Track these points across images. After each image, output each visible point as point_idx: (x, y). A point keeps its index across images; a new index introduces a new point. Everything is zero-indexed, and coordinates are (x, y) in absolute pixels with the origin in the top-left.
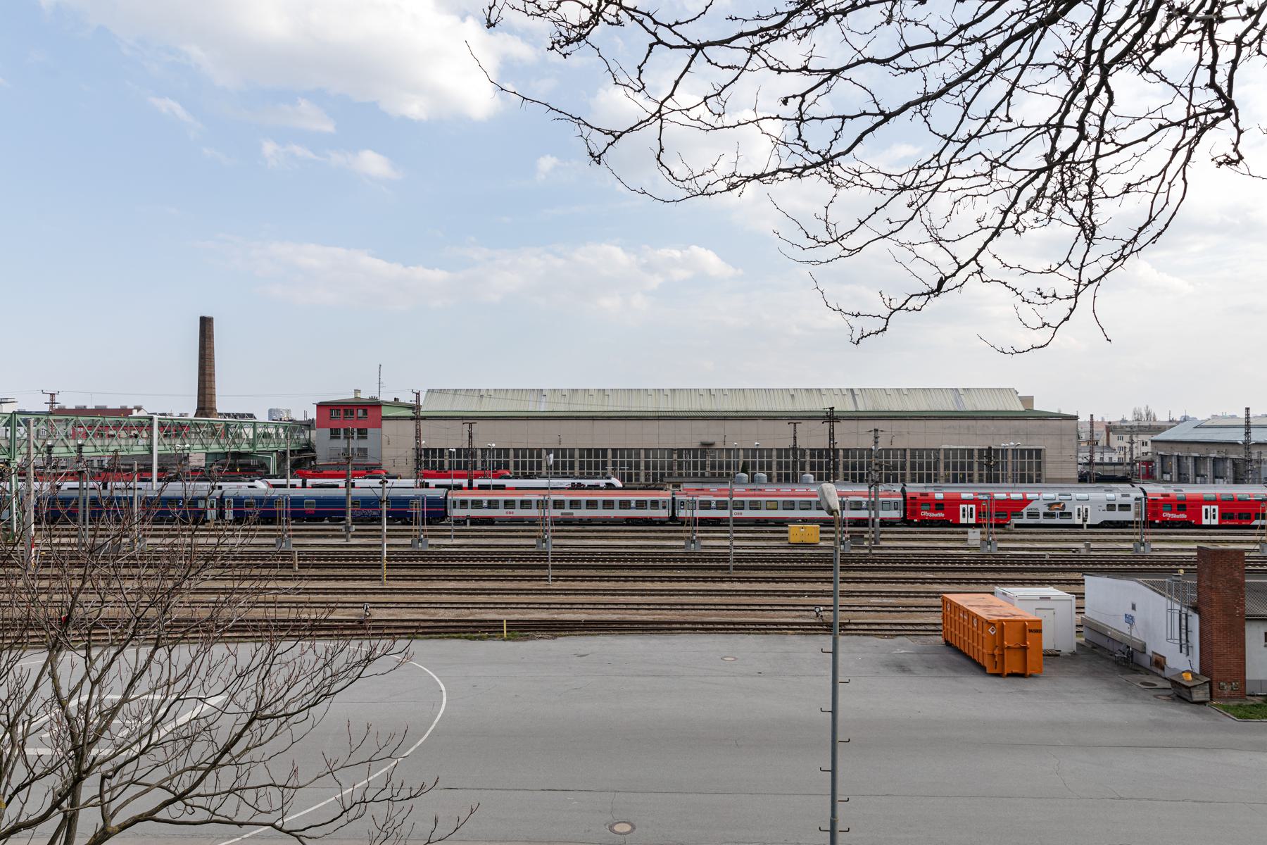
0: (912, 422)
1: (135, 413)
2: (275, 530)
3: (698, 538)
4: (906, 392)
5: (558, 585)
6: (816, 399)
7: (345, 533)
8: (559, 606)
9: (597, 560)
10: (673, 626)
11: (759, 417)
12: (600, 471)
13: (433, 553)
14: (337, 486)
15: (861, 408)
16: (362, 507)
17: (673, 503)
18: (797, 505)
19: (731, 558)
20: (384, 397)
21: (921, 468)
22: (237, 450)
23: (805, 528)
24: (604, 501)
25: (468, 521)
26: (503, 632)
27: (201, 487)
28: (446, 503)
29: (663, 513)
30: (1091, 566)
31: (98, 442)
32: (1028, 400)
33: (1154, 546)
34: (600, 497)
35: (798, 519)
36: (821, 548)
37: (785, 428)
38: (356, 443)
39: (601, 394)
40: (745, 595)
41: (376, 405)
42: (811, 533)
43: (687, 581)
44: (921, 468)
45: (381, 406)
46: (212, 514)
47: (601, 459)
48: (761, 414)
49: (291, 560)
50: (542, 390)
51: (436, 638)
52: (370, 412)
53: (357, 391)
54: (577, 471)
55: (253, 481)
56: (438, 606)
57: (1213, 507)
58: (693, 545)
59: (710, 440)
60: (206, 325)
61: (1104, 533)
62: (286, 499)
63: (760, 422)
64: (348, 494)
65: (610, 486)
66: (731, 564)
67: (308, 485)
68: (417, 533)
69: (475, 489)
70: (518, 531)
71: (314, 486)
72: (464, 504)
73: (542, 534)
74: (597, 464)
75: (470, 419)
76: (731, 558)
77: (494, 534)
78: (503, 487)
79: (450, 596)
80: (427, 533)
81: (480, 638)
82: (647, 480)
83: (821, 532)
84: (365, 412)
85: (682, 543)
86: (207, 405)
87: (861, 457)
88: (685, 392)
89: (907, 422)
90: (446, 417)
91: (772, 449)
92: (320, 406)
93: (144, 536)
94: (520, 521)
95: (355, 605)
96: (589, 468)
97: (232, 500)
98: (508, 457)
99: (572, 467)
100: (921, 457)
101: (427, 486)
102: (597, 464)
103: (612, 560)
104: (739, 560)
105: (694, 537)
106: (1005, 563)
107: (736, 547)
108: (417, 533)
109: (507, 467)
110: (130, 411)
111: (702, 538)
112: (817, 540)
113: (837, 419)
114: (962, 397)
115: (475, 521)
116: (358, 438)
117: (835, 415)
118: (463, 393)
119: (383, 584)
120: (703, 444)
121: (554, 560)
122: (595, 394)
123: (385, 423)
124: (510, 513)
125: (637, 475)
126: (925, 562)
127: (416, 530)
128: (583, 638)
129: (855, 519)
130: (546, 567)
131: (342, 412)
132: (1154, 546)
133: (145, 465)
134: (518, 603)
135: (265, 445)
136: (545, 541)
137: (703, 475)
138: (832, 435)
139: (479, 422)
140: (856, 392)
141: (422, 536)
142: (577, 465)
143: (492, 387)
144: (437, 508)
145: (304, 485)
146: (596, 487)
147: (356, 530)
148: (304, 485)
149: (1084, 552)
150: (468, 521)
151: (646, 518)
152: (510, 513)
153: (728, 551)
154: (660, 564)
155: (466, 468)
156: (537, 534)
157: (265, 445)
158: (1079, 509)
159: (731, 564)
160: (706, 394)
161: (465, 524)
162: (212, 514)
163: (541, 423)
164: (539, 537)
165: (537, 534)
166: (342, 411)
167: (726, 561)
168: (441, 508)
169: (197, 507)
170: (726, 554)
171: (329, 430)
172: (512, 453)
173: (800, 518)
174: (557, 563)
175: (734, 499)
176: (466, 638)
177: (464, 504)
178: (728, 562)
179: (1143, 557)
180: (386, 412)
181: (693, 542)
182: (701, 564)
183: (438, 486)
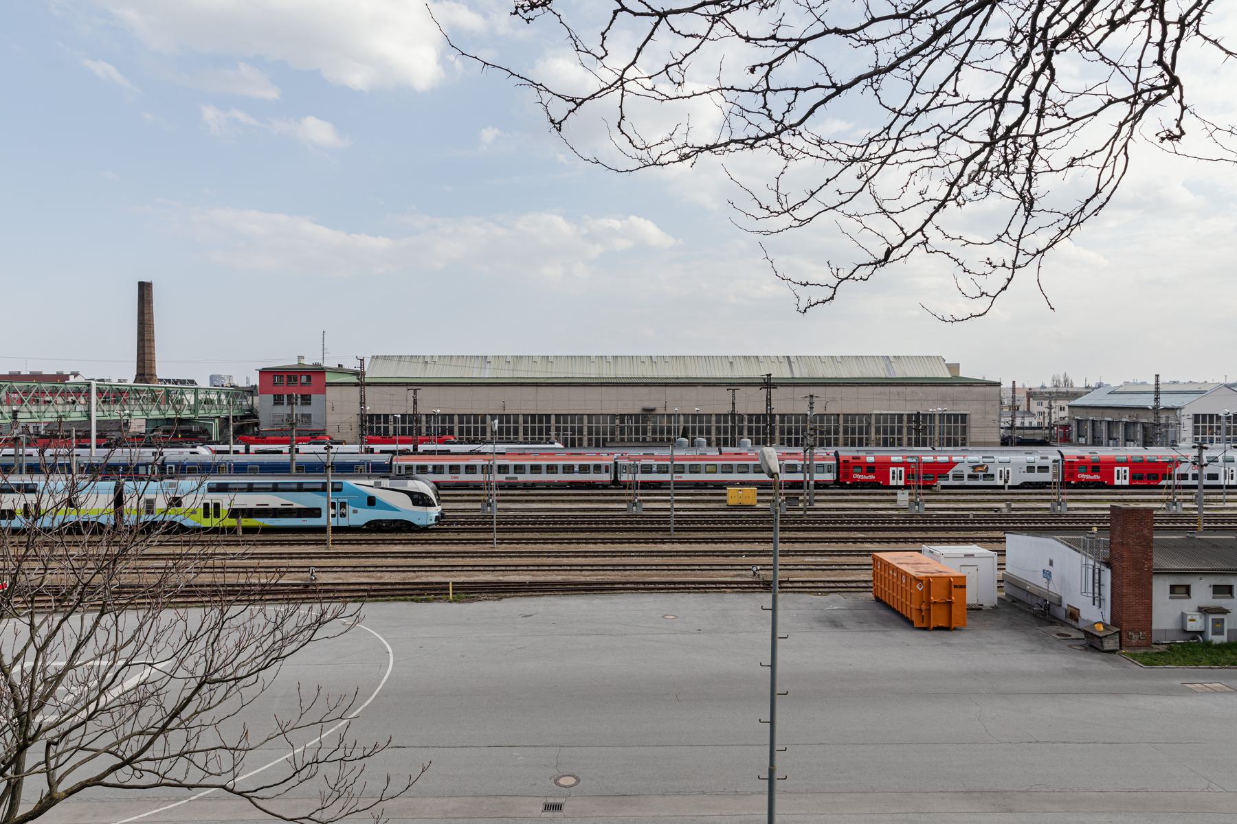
0: (844, 389)
1: (72, 379)
3: (639, 501)
5: (503, 548)
8: (504, 568)
13: (1186, 515)
14: (281, 452)
15: (797, 375)
18: (735, 469)
19: (672, 520)
23: (743, 490)
29: (606, 477)
31: (34, 408)
36: (759, 509)
37: (724, 394)
38: (299, 410)
39: (544, 360)
41: (319, 371)
42: (749, 496)
43: (629, 543)
50: (486, 357)
51: (382, 601)
52: (313, 378)
53: (300, 357)
56: (384, 569)
57: (1124, 468)
59: (651, 406)
60: (144, 289)
61: (1024, 494)
62: (230, 465)
64: (292, 460)
66: (672, 526)
70: (463, 495)
71: (257, 452)
73: (486, 498)
75: (414, 386)
76: (672, 520)
78: (447, 452)
81: (427, 601)
83: (758, 494)
84: (309, 379)
87: (797, 422)
90: (390, 383)
91: (711, 415)
92: (263, 372)
95: (301, 570)
96: (533, 433)
97: (173, 466)
103: (555, 523)
104: (679, 522)
107: (676, 510)
109: (451, 432)
110: (67, 377)
111: (644, 501)
112: (755, 502)
113: (775, 386)
116: (302, 404)
120: (644, 410)
122: (539, 361)
123: (328, 389)
135: (207, 411)
137: (644, 439)
138: (769, 401)
140: (792, 360)
145: (247, 451)
148: (247, 451)
149: (1005, 512)
151: (589, 482)
153: (669, 513)
154: (603, 526)
155: (410, 434)
156: (482, 498)
158: (1001, 471)
159: (672, 526)
163: (615, 389)
165: (482, 498)
166: (285, 377)
170: (667, 516)
173: (738, 481)
174: (502, 526)
176: (412, 600)
180: (329, 378)
181: (635, 504)
182: (642, 526)
183: (257, 452)
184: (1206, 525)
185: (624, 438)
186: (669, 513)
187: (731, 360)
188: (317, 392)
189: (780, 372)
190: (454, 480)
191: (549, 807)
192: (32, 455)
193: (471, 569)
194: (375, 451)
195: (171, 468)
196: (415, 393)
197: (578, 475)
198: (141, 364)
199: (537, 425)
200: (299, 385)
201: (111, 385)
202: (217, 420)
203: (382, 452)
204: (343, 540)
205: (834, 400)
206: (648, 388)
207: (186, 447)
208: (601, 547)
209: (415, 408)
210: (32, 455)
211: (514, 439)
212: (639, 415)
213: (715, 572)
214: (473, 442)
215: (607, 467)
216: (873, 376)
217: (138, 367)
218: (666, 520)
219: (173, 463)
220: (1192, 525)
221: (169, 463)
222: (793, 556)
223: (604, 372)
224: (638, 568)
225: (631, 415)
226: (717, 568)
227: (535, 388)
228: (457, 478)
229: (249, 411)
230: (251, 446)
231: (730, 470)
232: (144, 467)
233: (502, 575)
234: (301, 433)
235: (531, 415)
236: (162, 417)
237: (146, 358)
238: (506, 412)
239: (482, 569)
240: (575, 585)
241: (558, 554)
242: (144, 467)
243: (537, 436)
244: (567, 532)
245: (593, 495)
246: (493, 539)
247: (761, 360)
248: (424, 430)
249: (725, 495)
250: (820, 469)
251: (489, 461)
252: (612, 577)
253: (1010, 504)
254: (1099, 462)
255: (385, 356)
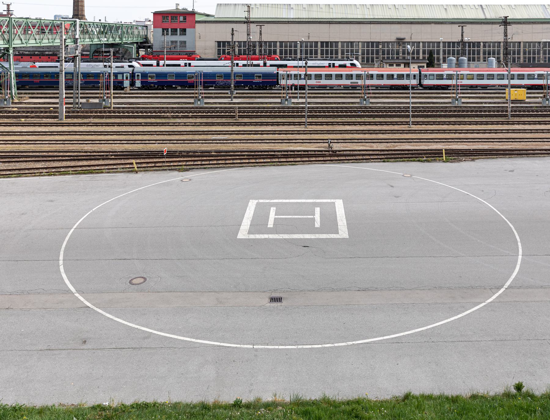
0: (524, 26)
2: (193, 93)
3: (460, 97)
4: (514, 7)
5: (414, 127)
6: (524, 10)
7: (230, 95)
8: (260, 141)
9: (276, 112)
10: (236, 153)
11: (432, 22)
12: (334, 56)
13: (207, 108)
14: (151, 65)
15: (488, 17)
16: (224, 79)
17: (420, 76)
18: (495, 77)
19: (509, 110)
20: (197, 10)
21: (529, 53)
22: (114, 42)
23: (518, 91)
24: (326, 75)
25: (293, 87)
26: (443, 156)
27: (97, 66)
28: (278, 76)
29: (414, 82)
30: (140, 114)
31: (50, 37)
32: (68, 16)
33: (464, 100)
34: (344, 72)
35: (496, 85)
37: (457, 29)
38: (178, 38)
39: (327, 7)
40: (356, 133)
41: (193, 14)
42: (521, 94)
43: (294, 125)
44: (529, 53)
45: (195, 14)
46: (127, 83)
47: (334, 48)
48: (433, 21)
49: (234, 113)
50: (290, 5)
51: (400, 161)
52: (188, 18)
53: (177, 5)
54: (340, 56)
55: (131, 62)
56: (225, 142)
58: (457, 102)
59: (402, 37)
62: (201, 74)
63: (433, 25)
64: (232, 71)
65: (353, 65)
67: (267, 65)
68: (285, 95)
69: (337, 67)
72: (289, 76)
73: (363, 95)
74: (332, 51)
75: (462, 23)
76: (509, 110)
77: (320, 95)
78: (285, 66)
79: (249, 136)
80: (291, 95)
82: (525, 61)
83: (527, 93)
84: (185, 19)
85: (450, 100)
86: (80, 13)
87: (494, 47)
88: (379, 6)
89: (521, 25)
90: (237, 21)
91: (277, 42)
92: (156, 14)
93: (202, 97)
94: (324, 87)
95: (534, 140)
96: (327, 53)
97: (140, 74)
98: (276, 47)
99: (337, 53)
100: (530, 46)
101: (35, 67)
102: (332, 51)
103: (262, 112)
104: (311, 112)
105: (366, 97)
106: (533, 111)
107: (309, 103)
108: (285, 95)
109: (275, 52)
111: (463, 97)
112: (525, 98)
113: (510, 23)
114: (548, 9)
115: (392, 87)
116: (172, 34)
117: (508, 21)
118: (240, 7)
119: (306, 127)
120: (397, 39)
121: (239, 112)
122: (324, 7)
123: (197, 25)
124: (318, 82)
125: (519, 58)
126: (346, 112)
127: (284, 93)
128: (489, 160)
129: (531, 85)
130: (408, 116)
131: (170, 18)
132: (464, 100)
133: (39, 51)
134: (163, 140)
135: (38, 41)
136: (104, 100)
137: (418, 58)
138: (506, 35)
139: (469, 26)
140: (484, 7)
141: (366, 97)
142: (340, 52)
143: (258, 2)
144: (272, 79)
145: (158, 65)
146: (344, 66)
147: (237, 93)
148: (158, 65)
150: (293, 87)
151: (403, 85)
152: (318, 82)
153: (304, 106)
154: (82, 114)
155: (244, 54)
157: (38, 41)
160: (392, 7)
161: (292, 89)
162: (127, 83)
163: (348, 26)
164: (362, 97)
165: (280, 95)
166: (170, 17)
167: (507, 111)
168: (275, 79)
169: (117, 79)
170: (303, 108)
171: (161, 29)
172: (278, 44)
173: (497, 85)
174: (241, 114)
175: (511, 73)
176: (419, 161)
177: (289, 76)
178: (507, 112)
179: (365, 107)
180: (198, 18)
181: (365, 100)
182: (322, 114)
183: (271, 66)
184: (309, 114)
185: (385, 57)
186: (304, 106)
187: (445, 7)
188: (190, 27)
189: (512, 15)
190: (317, 84)
191: (274, 300)
192: (123, 67)
193: (168, 142)
194: (239, 65)
195: (138, 76)
196: (261, 28)
197: (397, 80)
198: (76, 8)
199: (325, 48)
200: (178, 22)
201: (101, 23)
202: (135, 45)
203: (271, 66)
204: (334, 122)
205: (518, 33)
206: (400, 25)
207: (125, 62)
208: (302, 128)
209: (260, 38)
210: (123, 67)
211: (315, 57)
212: (394, 42)
213: (66, 145)
214: (284, 60)
215: (415, 76)
216: (536, 18)
217: (74, 10)
218: (406, 110)
219: (139, 73)
220: (504, 113)
221: (137, 73)
222: (448, 133)
223: (386, 15)
224: (164, 142)
225: (454, 42)
226: (76, 142)
227: (328, 25)
228: (320, 82)
229: (145, 39)
230: (160, 61)
231: (482, 78)
232: (121, 75)
233: (448, 145)
234: (181, 53)
235: (326, 42)
236: (99, 43)
237: (79, 4)
238: (310, 40)
239: (260, 141)
240: (504, 151)
241: (274, 132)
242: (121, 75)
243: (334, 56)
244: (482, 117)
245: (432, 93)
246: (409, 122)
247: (464, 7)
248: (257, 51)
249: (58, 93)
250: (431, 77)
251: (365, 71)
252: (518, 146)
253: (88, 100)
254: (207, 74)
255: (226, 4)
